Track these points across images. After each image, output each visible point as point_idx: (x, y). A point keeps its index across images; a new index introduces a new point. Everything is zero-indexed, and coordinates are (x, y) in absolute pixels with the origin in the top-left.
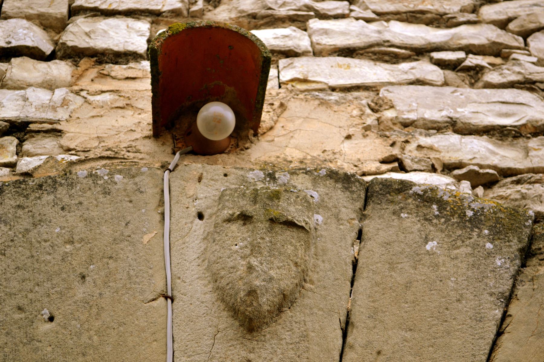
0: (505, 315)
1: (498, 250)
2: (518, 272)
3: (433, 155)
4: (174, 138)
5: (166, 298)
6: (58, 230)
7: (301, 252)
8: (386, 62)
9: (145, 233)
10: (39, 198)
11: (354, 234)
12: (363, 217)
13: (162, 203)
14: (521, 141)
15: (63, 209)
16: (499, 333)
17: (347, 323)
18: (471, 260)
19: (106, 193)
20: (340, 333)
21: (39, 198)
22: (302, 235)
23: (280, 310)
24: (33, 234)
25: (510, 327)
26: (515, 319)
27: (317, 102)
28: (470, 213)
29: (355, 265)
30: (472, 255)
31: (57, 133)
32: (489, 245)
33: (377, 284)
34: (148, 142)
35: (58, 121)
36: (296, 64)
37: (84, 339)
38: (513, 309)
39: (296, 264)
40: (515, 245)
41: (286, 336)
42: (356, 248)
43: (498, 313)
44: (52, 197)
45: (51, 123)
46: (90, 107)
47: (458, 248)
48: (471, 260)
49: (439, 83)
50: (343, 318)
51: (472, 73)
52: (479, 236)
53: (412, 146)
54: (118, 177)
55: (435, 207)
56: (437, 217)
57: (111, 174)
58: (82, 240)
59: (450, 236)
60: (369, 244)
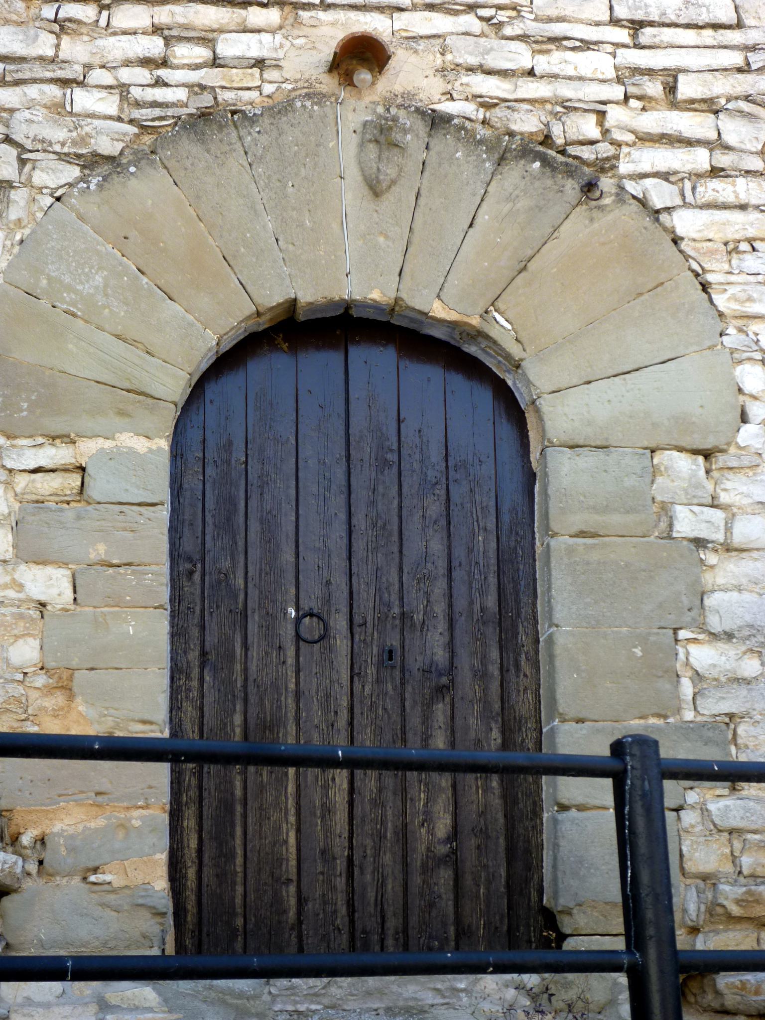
0: (486, 192)
1: (488, 159)
2: (495, 170)
3: (468, 89)
4: (339, 74)
5: (341, 177)
6: (291, 138)
7: (400, 160)
8: (451, 14)
9: (330, 142)
10: (280, 119)
11: (425, 146)
12: (430, 136)
13: (337, 123)
14: (514, 79)
15: (292, 126)
16: (482, 200)
17: (418, 193)
18: (475, 163)
19: (311, 117)
20: (415, 198)
21: (280, 119)
22: (401, 150)
23: (390, 187)
24: (280, 140)
25: (487, 199)
26: (490, 193)
27: (412, 51)
28: (478, 137)
29: (424, 163)
30: (476, 160)
31: (278, 67)
32: (485, 156)
33: (433, 174)
34: (325, 75)
35: (279, 60)
36: (402, 18)
37: (308, 197)
38: (490, 189)
39: (398, 166)
40: (497, 156)
41: (392, 199)
42: (425, 154)
43: (483, 191)
44: (286, 118)
45: (276, 60)
46: (294, 49)
47: (470, 156)
48: (475, 163)
49: (478, 34)
50: (417, 191)
51: (497, 26)
52: (481, 150)
53: (457, 84)
54: (316, 108)
55: (463, 132)
56: (463, 138)
57: (312, 106)
58: (302, 144)
59: (467, 150)
60: (432, 153)
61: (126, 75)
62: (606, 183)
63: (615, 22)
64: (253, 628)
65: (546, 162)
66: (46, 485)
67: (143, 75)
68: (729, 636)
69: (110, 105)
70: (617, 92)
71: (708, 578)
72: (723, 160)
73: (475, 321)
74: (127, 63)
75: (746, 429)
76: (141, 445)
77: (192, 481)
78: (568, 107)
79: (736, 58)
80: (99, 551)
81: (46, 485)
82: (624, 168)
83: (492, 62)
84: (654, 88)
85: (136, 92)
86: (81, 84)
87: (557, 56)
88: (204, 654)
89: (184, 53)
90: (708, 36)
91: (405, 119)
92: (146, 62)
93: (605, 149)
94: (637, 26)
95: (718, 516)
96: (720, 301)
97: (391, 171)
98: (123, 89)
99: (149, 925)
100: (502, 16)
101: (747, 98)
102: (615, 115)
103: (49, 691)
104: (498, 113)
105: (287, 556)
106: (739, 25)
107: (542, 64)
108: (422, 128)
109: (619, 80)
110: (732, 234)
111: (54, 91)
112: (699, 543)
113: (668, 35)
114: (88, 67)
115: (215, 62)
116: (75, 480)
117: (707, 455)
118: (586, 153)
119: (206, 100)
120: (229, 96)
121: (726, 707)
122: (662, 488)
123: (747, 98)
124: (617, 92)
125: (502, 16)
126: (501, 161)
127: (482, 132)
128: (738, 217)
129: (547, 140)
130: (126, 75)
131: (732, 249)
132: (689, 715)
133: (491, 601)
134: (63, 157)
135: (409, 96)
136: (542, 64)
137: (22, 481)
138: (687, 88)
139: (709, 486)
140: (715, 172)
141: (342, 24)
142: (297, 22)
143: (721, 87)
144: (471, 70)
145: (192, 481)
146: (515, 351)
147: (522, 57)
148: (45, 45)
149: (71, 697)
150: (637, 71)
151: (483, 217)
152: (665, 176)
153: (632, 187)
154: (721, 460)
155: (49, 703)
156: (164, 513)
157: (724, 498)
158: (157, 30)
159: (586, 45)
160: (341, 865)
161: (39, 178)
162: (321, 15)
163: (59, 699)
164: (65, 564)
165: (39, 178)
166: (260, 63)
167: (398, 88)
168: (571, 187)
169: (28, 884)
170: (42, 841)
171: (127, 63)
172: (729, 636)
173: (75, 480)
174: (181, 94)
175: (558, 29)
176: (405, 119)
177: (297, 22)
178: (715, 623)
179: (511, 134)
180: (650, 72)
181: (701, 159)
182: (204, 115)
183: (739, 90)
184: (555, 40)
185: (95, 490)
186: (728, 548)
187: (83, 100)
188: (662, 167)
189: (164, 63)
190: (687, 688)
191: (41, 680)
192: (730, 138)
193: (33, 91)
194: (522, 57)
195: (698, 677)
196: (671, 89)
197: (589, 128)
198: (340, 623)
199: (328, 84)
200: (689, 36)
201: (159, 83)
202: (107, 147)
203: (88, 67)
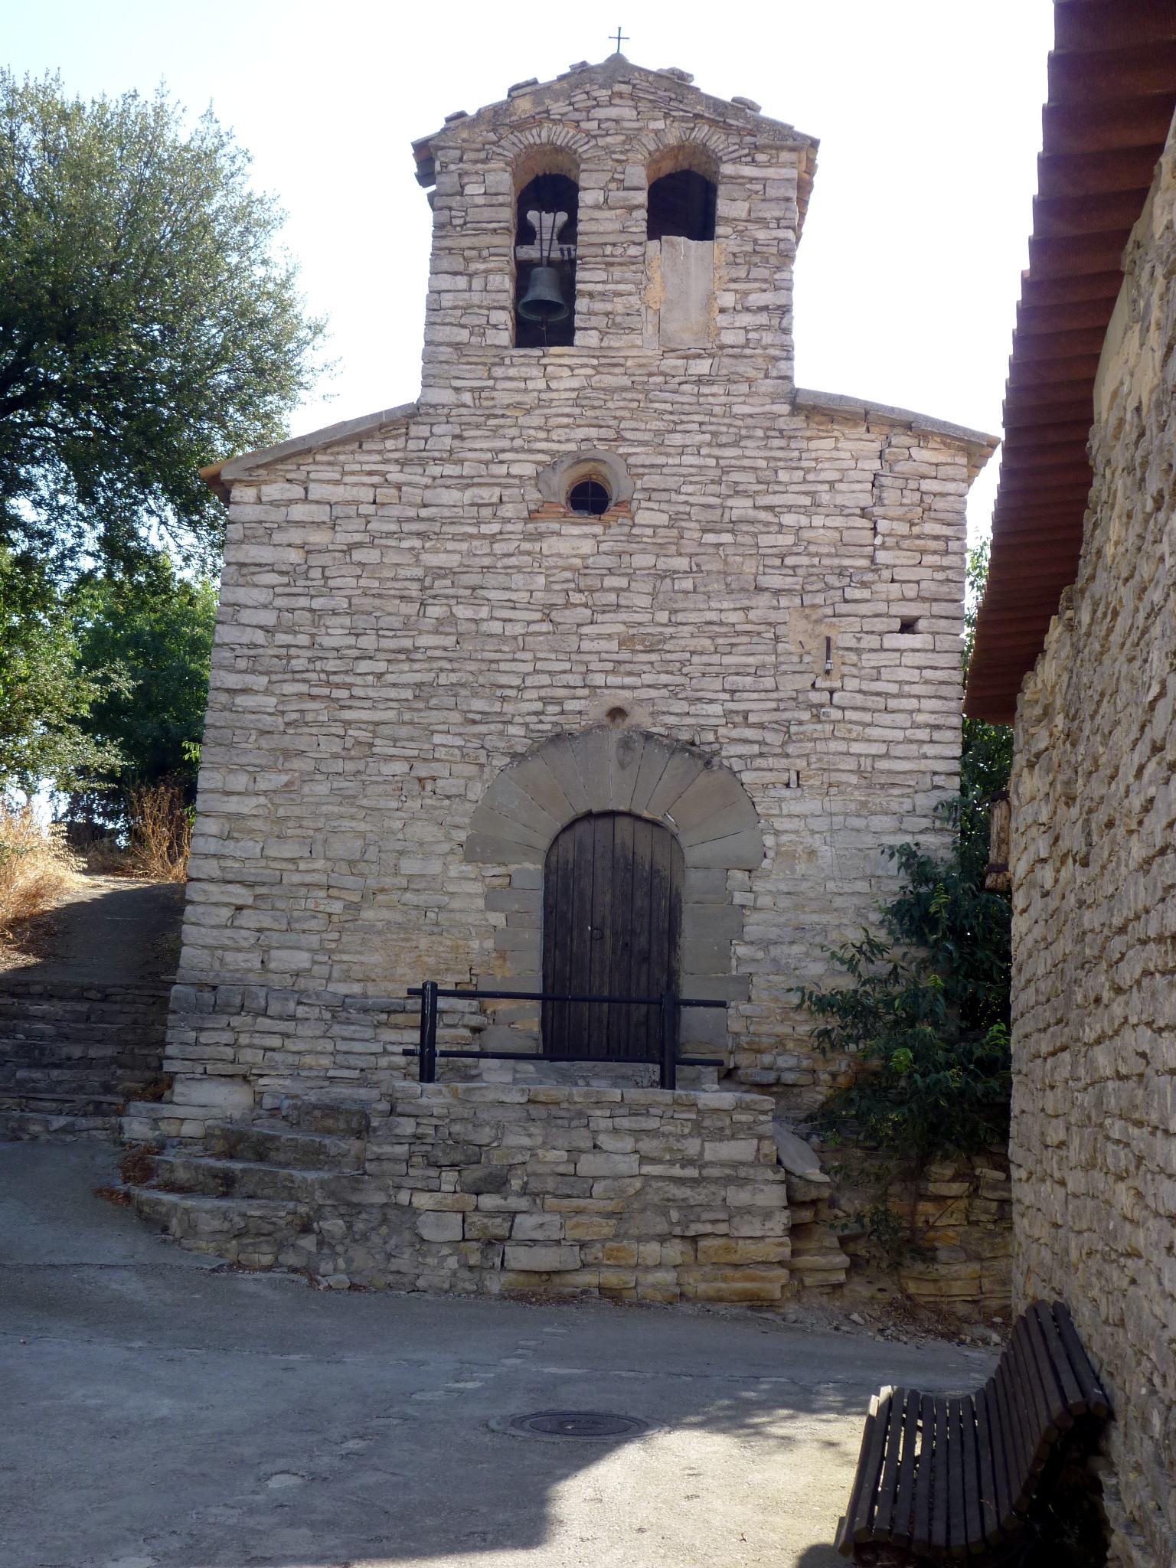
61: (528, 719)
62: (716, 760)
63: (724, 690)
64: (575, 933)
65: (691, 753)
66: (497, 882)
67: (534, 719)
68: (752, 943)
69: (521, 732)
70: (723, 721)
71: (746, 920)
72: (765, 749)
73: (660, 818)
74: (528, 714)
75: (766, 861)
76: (531, 867)
77: (553, 878)
78: (703, 728)
79: (773, 705)
80: (516, 907)
81: (497, 882)
82: (724, 753)
83: (673, 709)
84: (739, 719)
85: (532, 726)
86: (511, 723)
87: (699, 706)
88: (556, 943)
89: (552, 709)
90: (763, 695)
91: (635, 737)
92: (536, 713)
93: (716, 746)
94: (733, 692)
95: (752, 896)
96: (759, 809)
97: (628, 759)
98: (526, 725)
99: (533, 1044)
100: (678, 689)
101: (776, 722)
102: (722, 731)
103: (497, 958)
104: (674, 731)
105: (588, 907)
106: (777, 689)
107: (693, 709)
108: (642, 740)
109: (725, 716)
110: (765, 781)
111: (500, 726)
112: (743, 906)
113: (746, 695)
114: (513, 716)
115: (562, 713)
116: (507, 880)
117: (750, 871)
118: (707, 749)
119: (558, 729)
120: (567, 727)
121: (749, 970)
122: (730, 884)
123: (776, 722)
124: (723, 721)
125: (678, 689)
126: (673, 753)
127: (666, 741)
128: (769, 774)
129: (693, 744)
130: (528, 719)
131: (765, 787)
132: (734, 973)
133: (666, 925)
134: (503, 754)
135: (638, 726)
136: (693, 709)
137: (488, 880)
138: (752, 719)
139: (749, 883)
140: (761, 755)
141: (502, 956)
142: (595, 695)
143: (766, 718)
144: (664, 713)
145: (553, 878)
146: (675, 830)
147: (684, 707)
148: (497, 707)
149: (505, 960)
150: (732, 712)
151: (665, 776)
152: (740, 757)
153: (726, 762)
154: (754, 873)
155: (497, 963)
156: (541, 893)
157: (755, 888)
158: (540, 699)
159: (712, 701)
160: (605, 1023)
161: (495, 762)
162: (606, 691)
163: (500, 962)
164: (502, 911)
165: (495, 762)
166: (580, 712)
167: (634, 723)
168: (700, 763)
169: (490, 1028)
170: (494, 1012)
171: (528, 714)
172: (752, 943)
173: (507, 880)
174: (548, 727)
175: (700, 694)
176: (635, 737)
177: (595, 695)
178: (747, 938)
179: (678, 740)
180: (737, 712)
181: (756, 749)
182: (558, 735)
183: (774, 719)
184: (699, 699)
185: (514, 885)
186: (755, 908)
187: (512, 730)
188: (739, 753)
189: (543, 713)
190: (734, 962)
191: (494, 955)
192: (768, 740)
193: (492, 727)
194: (684, 707)
195: (739, 959)
196: (746, 718)
197: (711, 737)
198: (608, 932)
199: (606, 721)
200: (755, 696)
201: (541, 722)
202: (520, 749)
203: (513, 716)
